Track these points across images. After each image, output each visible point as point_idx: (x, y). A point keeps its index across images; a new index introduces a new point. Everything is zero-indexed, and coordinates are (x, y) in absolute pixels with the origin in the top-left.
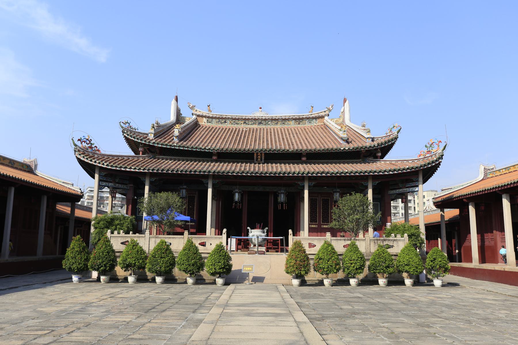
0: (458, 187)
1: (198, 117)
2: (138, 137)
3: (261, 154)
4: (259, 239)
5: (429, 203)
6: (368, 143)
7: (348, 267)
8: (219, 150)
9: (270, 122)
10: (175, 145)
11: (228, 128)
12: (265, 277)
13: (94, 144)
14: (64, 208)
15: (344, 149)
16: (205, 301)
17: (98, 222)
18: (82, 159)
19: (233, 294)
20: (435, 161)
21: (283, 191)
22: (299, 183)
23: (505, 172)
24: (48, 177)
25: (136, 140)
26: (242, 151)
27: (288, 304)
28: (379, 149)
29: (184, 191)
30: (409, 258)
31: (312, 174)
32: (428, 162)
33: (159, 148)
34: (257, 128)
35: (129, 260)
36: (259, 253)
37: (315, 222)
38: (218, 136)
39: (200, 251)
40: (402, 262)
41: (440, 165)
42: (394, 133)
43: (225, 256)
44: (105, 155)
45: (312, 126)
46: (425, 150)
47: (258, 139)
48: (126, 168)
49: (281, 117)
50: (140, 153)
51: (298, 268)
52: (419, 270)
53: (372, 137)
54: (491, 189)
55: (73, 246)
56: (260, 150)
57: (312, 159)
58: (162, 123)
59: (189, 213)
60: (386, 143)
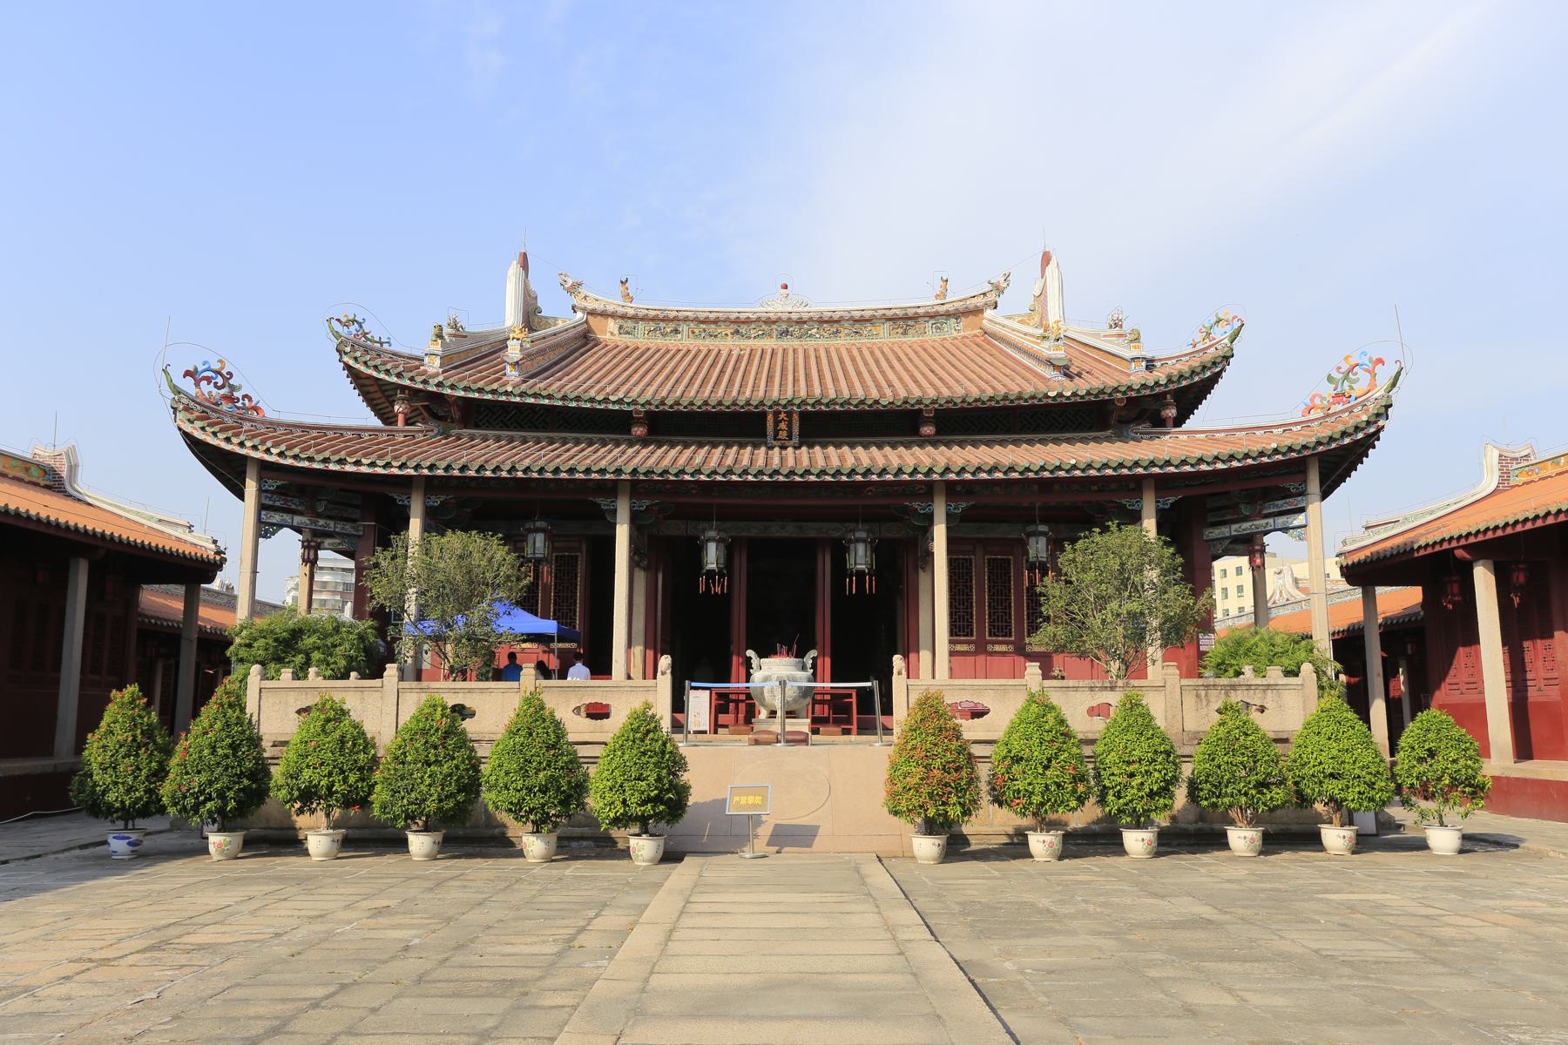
0: (1416, 517)
1: (589, 317)
2: (389, 366)
3: (789, 414)
4: (787, 689)
5: (1281, 581)
6: (1137, 376)
7: (1118, 787)
8: (650, 404)
9: (815, 330)
10: (509, 389)
11: (685, 349)
13: (239, 388)
14: (163, 601)
15: (1060, 395)
17: (248, 641)
18: (199, 435)
19: (687, 921)
20: (1363, 425)
21: (863, 535)
22: (916, 505)
24: (110, 504)
26: (728, 407)
28: (1169, 396)
30: (1339, 751)
31: (958, 474)
32: (1341, 428)
33: (460, 403)
34: (775, 347)
35: (307, 774)
37: (967, 635)
38: (650, 369)
39: (571, 738)
40: (1314, 766)
41: (1378, 439)
42: (1218, 343)
43: (663, 752)
44: (280, 424)
45: (945, 339)
46: (1328, 390)
49: (849, 312)
50: (397, 421)
51: (937, 794)
52: (1378, 796)
53: (1149, 356)
55: (109, 726)
56: (784, 402)
57: (953, 432)
58: (472, 326)
59: (559, 610)
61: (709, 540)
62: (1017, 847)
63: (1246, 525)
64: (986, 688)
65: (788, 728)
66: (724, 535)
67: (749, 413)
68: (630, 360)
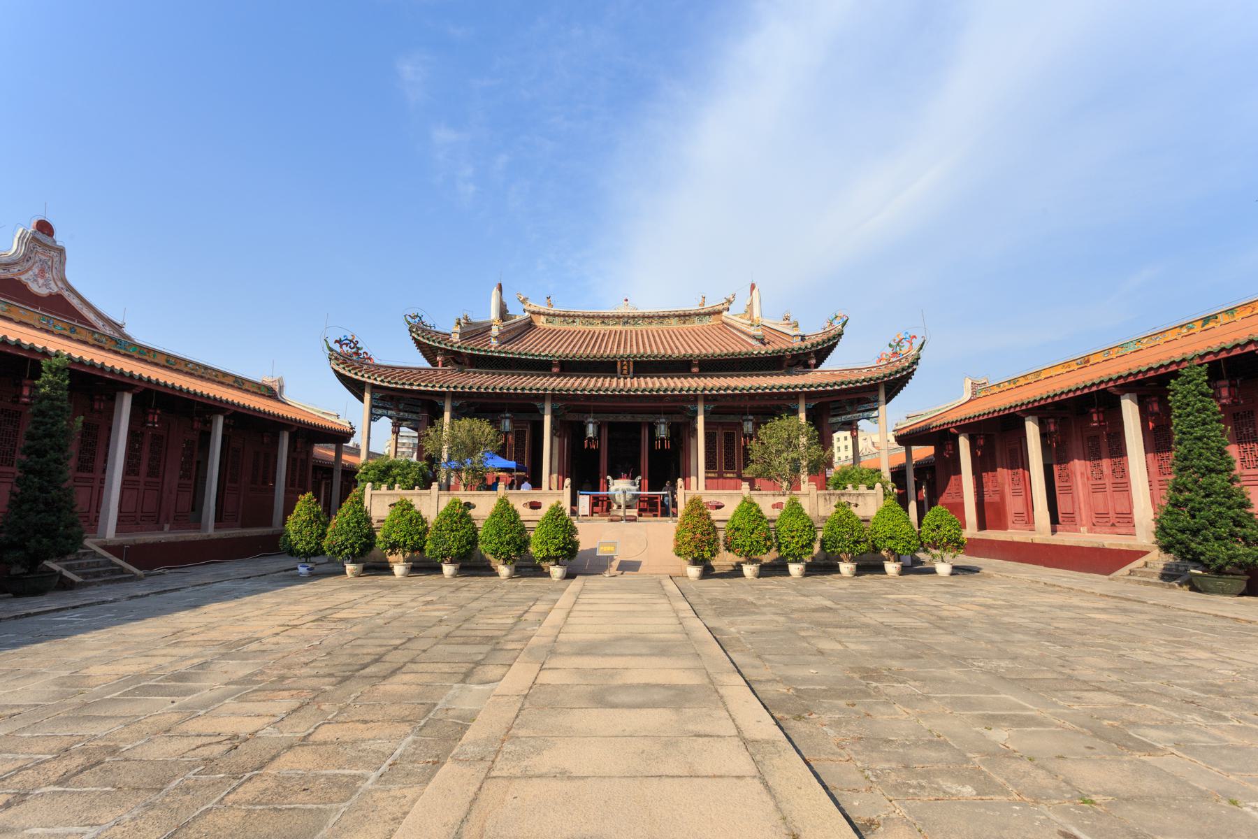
0: (931, 412)
2: (434, 338)
3: (628, 362)
6: (797, 344)
10: (493, 349)
12: (641, 562)
13: (362, 349)
14: (324, 452)
15: (759, 353)
16: (511, 630)
18: (342, 371)
19: (577, 608)
21: (664, 420)
22: (689, 406)
23: (1010, 387)
25: (431, 343)
27: (696, 642)
29: (507, 422)
31: (710, 391)
32: (895, 369)
36: (627, 520)
39: (522, 518)
43: (566, 526)
46: (889, 351)
47: (623, 343)
48: (411, 384)
53: (802, 334)
54: (1005, 409)
60: (824, 342)
61: (589, 423)
62: (737, 572)
63: (849, 416)
64: (723, 494)
65: (627, 514)
66: (596, 420)
67: (609, 362)
68: (551, 336)
